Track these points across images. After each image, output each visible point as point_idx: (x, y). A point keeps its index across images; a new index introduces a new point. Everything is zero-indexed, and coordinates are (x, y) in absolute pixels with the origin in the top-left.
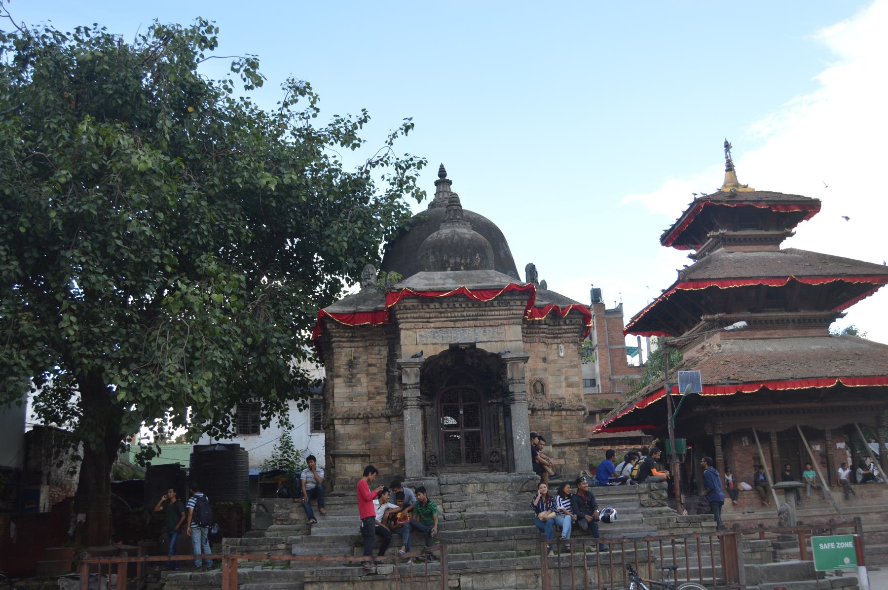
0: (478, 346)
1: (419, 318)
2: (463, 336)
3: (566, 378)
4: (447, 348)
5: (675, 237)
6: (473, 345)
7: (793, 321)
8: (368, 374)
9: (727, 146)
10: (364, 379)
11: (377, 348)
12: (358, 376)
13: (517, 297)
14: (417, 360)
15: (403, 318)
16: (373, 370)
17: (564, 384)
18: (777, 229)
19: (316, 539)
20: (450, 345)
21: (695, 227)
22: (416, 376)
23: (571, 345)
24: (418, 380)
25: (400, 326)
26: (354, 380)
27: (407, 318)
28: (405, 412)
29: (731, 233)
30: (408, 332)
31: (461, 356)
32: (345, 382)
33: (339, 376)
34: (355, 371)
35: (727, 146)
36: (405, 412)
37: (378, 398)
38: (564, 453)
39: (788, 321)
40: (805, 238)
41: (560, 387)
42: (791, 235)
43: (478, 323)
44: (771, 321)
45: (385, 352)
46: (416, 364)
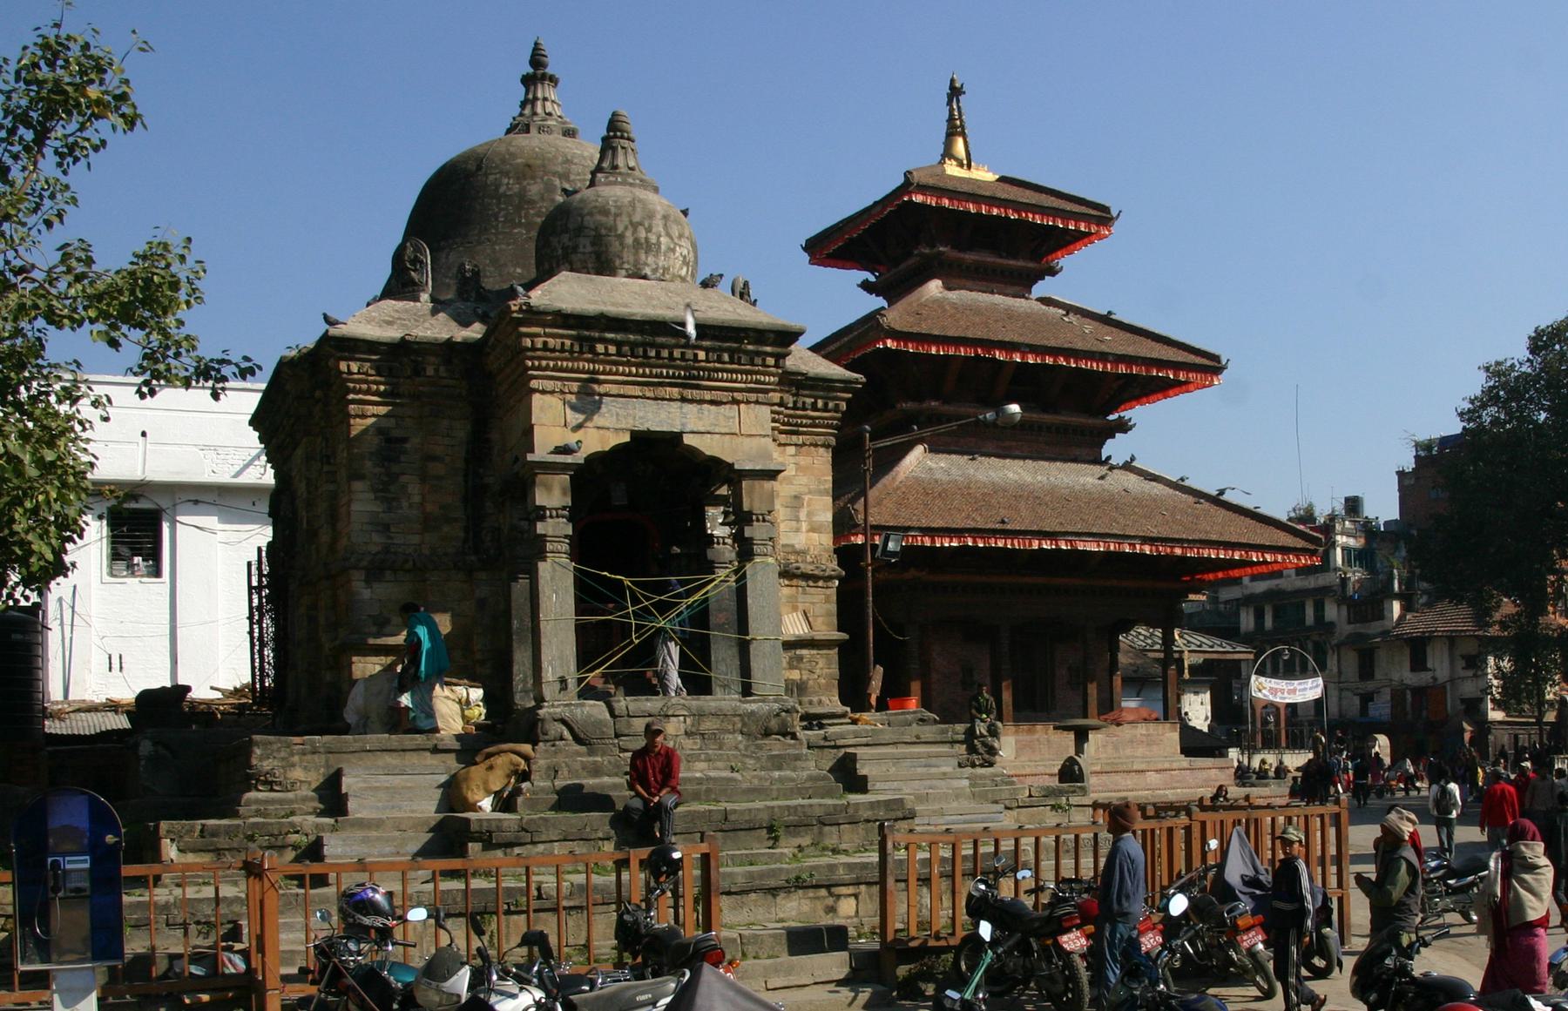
0: (688, 440)
1: (572, 371)
2: (661, 416)
3: (809, 514)
4: (627, 438)
5: (830, 248)
6: (678, 436)
7: (1049, 428)
8: (423, 479)
9: (955, 92)
10: (414, 490)
11: (445, 423)
12: (404, 479)
13: (768, 349)
14: (569, 459)
15: (539, 368)
16: (436, 469)
17: (804, 526)
18: (1031, 259)
19: (362, 824)
20: (634, 434)
21: (892, 238)
22: (564, 494)
23: (821, 450)
24: (568, 501)
25: (534, 384)
26: (392, 488)
27: (547, 368)
28: (541, 565)
29: (955, 254)
30: (548, 398)
31: (654, 454)
32: (375, 491)
33: (361, 477)
34: (395, 468)
35: (955, 92)
36: (541, 565)
37: (446, 529)
38: (801, 658)
39: (1040, 428)
40: (1079, 279)
41: (798, 530)
42: (1053, 272)
43: (689, 393)
45: (462, 431)
46: (564, 468)
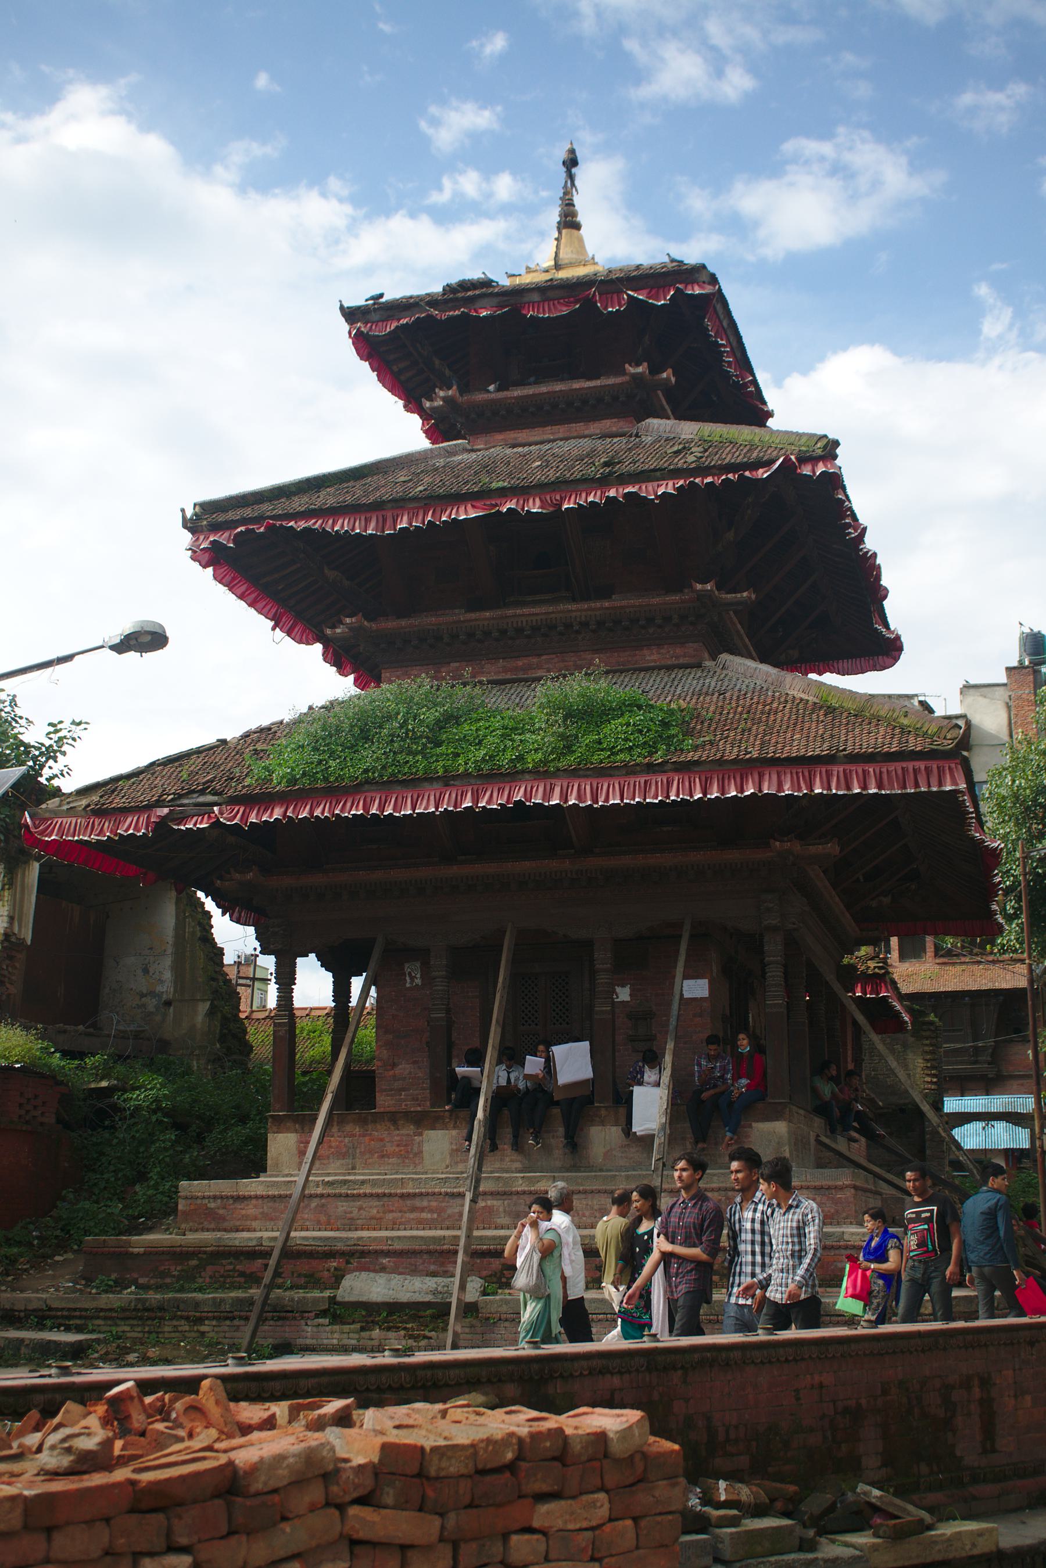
7: (585, 624)
44: (520, 631)
